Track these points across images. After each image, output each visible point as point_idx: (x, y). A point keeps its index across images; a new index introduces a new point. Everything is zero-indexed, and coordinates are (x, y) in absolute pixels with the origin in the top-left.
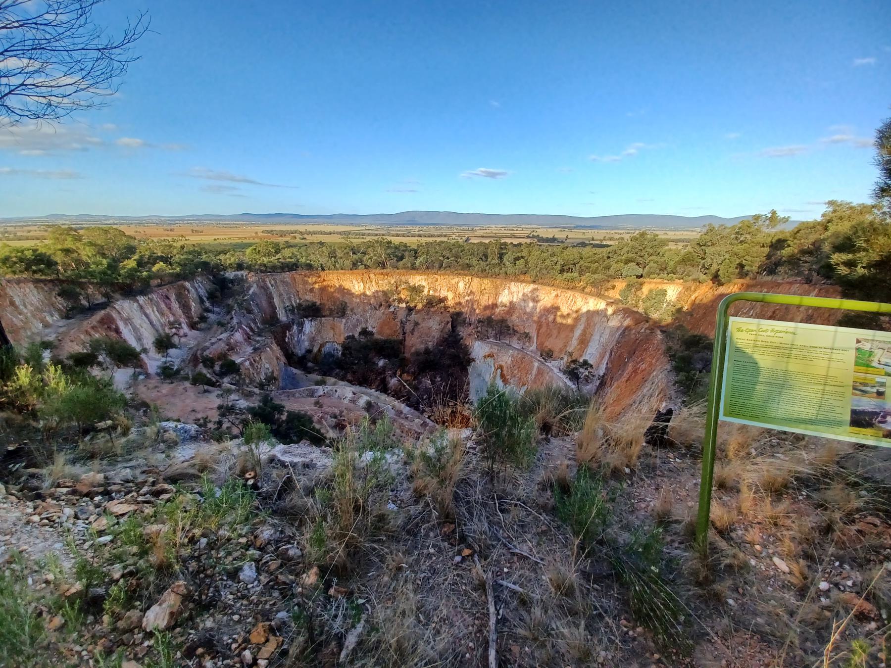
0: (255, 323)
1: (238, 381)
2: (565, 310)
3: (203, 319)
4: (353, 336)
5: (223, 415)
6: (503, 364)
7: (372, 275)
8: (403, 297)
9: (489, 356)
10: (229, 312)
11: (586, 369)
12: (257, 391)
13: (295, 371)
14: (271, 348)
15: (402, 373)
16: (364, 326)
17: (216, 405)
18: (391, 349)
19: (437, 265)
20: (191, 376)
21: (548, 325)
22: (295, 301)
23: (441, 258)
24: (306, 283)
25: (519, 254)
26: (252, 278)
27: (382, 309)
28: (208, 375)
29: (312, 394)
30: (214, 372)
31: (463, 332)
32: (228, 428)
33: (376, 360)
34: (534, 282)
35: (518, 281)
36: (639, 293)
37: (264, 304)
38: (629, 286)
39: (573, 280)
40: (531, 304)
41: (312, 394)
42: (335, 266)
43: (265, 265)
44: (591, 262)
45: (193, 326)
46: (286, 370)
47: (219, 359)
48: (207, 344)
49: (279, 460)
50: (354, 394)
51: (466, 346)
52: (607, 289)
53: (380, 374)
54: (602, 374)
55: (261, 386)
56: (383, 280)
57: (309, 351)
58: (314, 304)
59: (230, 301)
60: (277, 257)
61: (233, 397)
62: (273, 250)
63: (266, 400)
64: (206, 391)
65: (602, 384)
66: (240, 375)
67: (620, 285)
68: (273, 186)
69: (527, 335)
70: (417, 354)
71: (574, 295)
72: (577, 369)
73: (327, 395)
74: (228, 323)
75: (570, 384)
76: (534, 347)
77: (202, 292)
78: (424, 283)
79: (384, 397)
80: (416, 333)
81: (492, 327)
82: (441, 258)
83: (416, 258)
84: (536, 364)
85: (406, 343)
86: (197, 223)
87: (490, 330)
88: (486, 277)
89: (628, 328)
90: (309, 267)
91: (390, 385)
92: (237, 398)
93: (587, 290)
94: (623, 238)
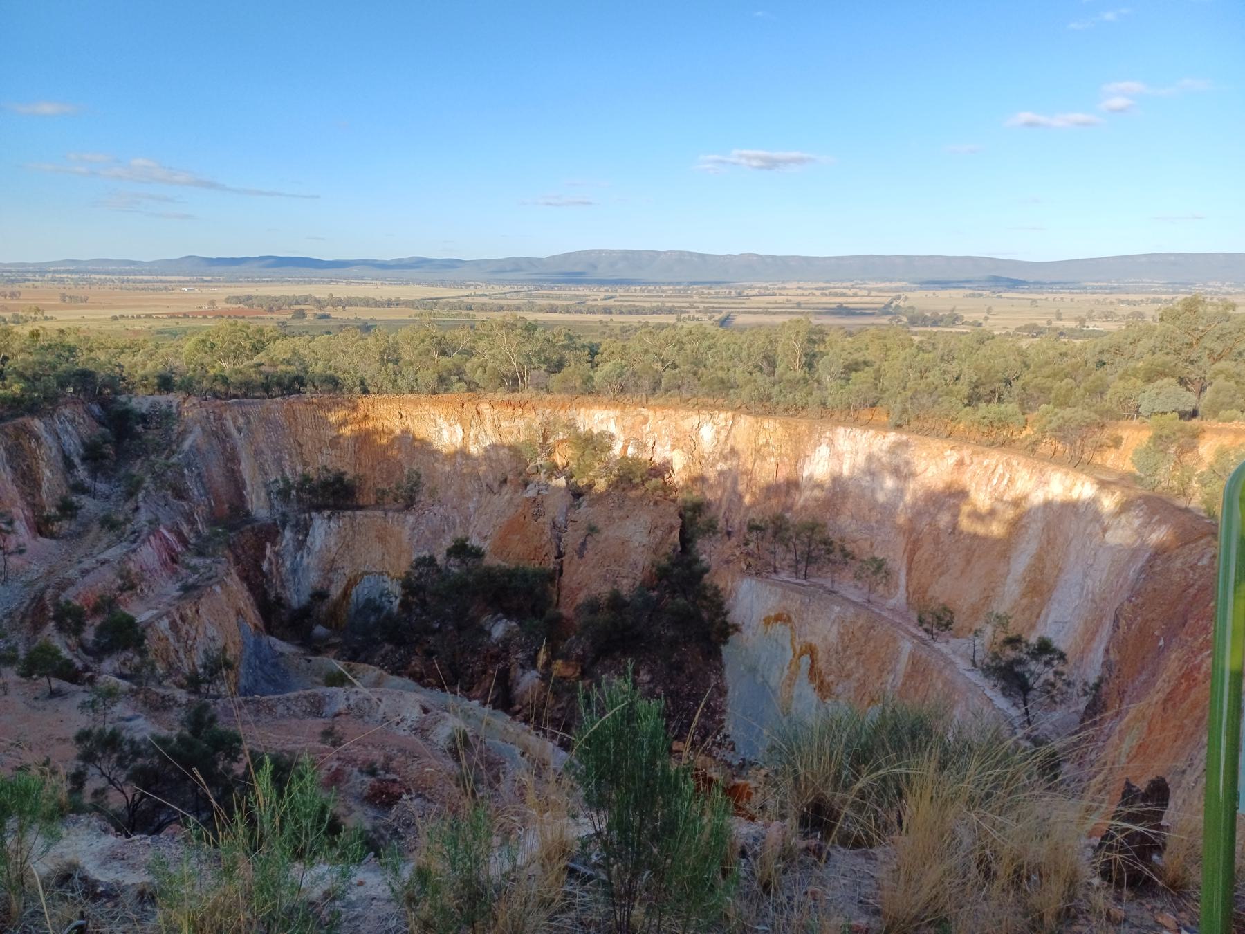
0: (191, 522)
1: (138, 670)
2: (982, 499)
3: (67, 509)
4: (432, 560)
5: (88, 757)
6: (816, 641)
7: (485, 407)
8: (559, 460)
9: (778, 618)
10: (131, 494)
11: (1047, 664)
12: (181, 695)
13: (281, 646)
14: (222, 583)
15: (553, 655)
16: (460, 534)
17: (73, 732)
18: (524, 593)
19: (646, 382)
20: (22, 654)
21: (936, 540)
22: (294, 469)
23: (658, 366)
24: (324, 422)
25: (858, 357)
26: (191, 410)
27: (508, 490)
28: (65, 653)
29: (316, 707)
30: (81, 645)
31: (708, 552)
32: (96, 793)
33: (486, 619)
34: (898, 427)
35: (856, 423)
36: (1187, 458)
37: (217, 473)
38: (1161, 441)
39: (1003, 422)
40: (889, 483)
41: (316, 707)
42: (394, 382)
43: (225, 380)
44: (1054, 375)
45: (41, 527)
46: (258, 644)
47: (96, 610)
48: (72, 573)
49: (84, 879)
50: (426, 711)
51: (717, 593)
52: (1099, 448)
53: (496, 658)
54: (1093, 680)
55: (193, 683)
56: (513, 418)
57: (320, 595)
58: (339, 478)
59: (137, 468)
60: (256, 360)
61: (120, 709)
62: (247, 344)
63: (199, 720)
64: (54, 694)
65: (1095, 708)
66: (143, 653)
67: (1135, 437)
68: (260, 193)
69: (879, 567)
70: (593, 607)
71: (1009, 464)
72: (1020, 662)
73: (357, 712)
74: (128, 520)
75: (1002, 703)
76: (899, 598)
77: (73, 444)
78: (612, 428)
79: (501, 721)
80: (588, 554)
81: (785, 542)
82: (658, 366)
83: (595, 366)
84: (907, 646)
85: (565, 580)
86: (79, 280)
87: (780, 550)
88: (771, 413)
89: (1160, 552)
90: (334, 383)
91: (518, 690)
92: (129, 714)
93: (1046, 447)
94: (1141, 315)
